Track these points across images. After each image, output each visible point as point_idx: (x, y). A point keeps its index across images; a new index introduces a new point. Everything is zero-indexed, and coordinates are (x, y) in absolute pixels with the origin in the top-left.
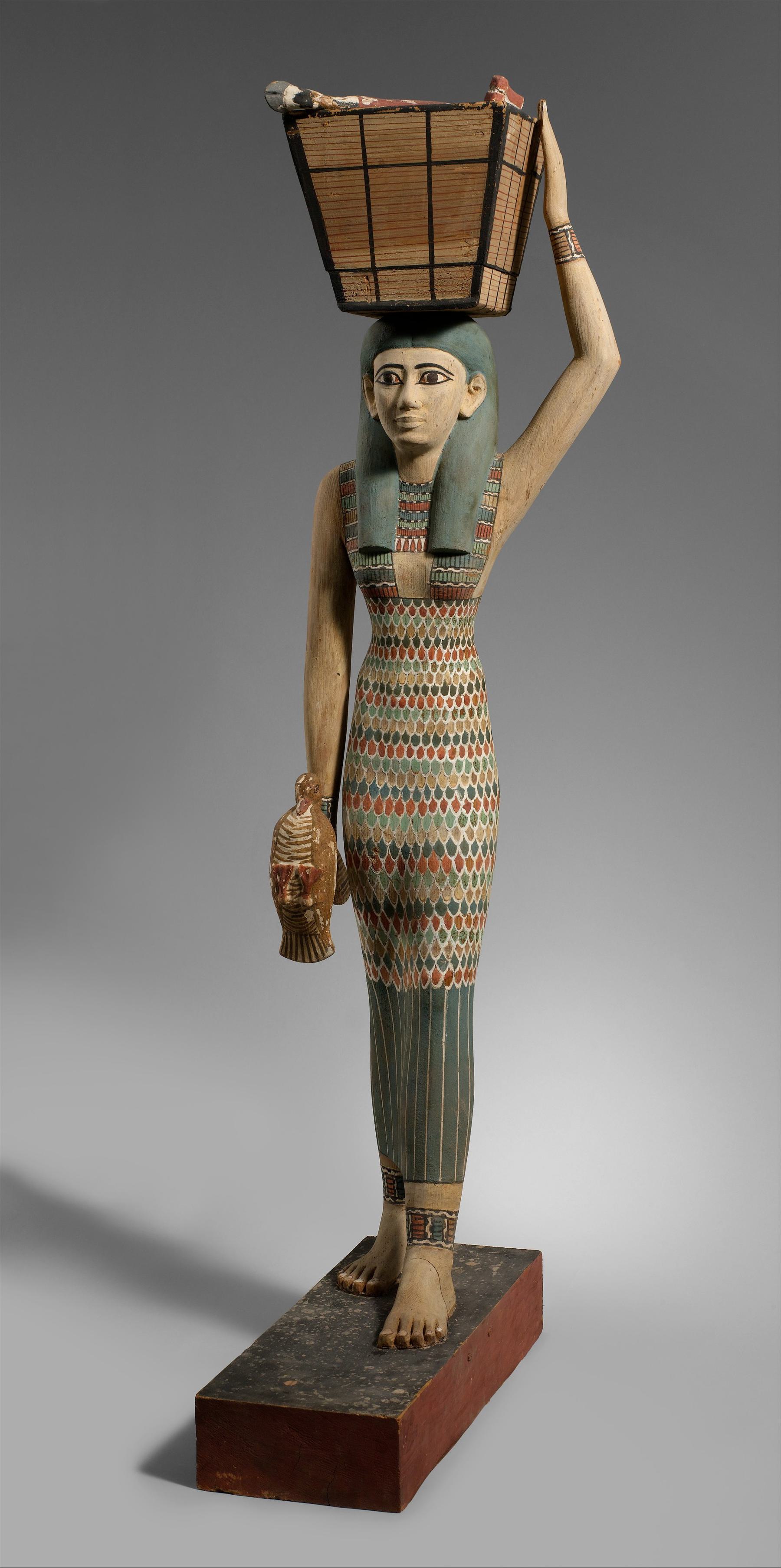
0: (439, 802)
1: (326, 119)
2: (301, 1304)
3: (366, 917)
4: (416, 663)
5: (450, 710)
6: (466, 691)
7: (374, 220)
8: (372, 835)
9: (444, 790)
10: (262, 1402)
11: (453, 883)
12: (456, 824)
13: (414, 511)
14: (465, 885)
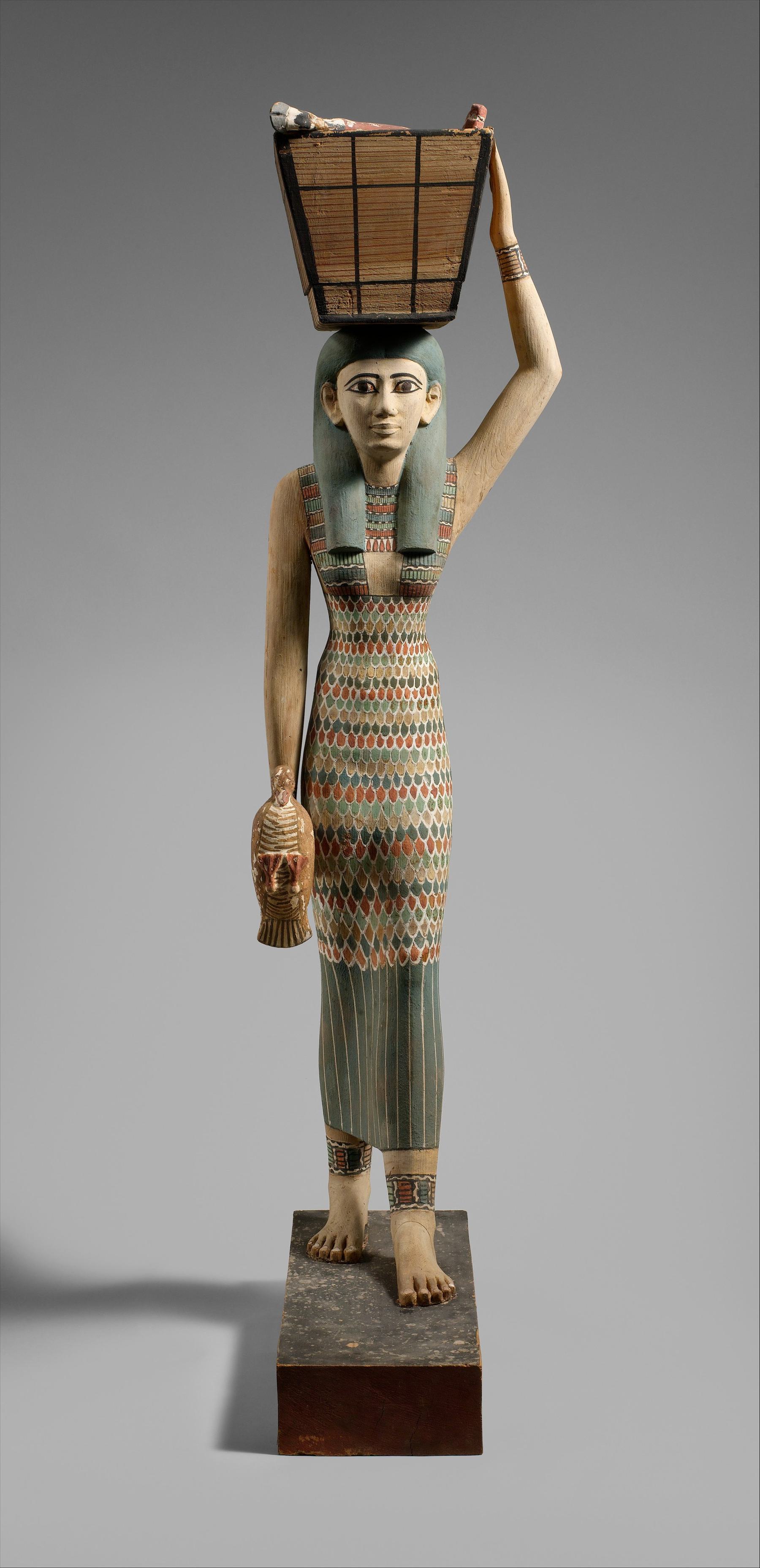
0: (409, 788)
1: (318, 140)
2: (292, 1276)
3: (331, 902)
4: (385, 657)
5: (416, 701)
6: (428, 683)
7: (360, 236)
8: (343, 822)
9: (413, 776)
10: (344, 1364)
11: (427, 865)
12: (426, 808)
13: (381, 513)
14: (436, 866)
